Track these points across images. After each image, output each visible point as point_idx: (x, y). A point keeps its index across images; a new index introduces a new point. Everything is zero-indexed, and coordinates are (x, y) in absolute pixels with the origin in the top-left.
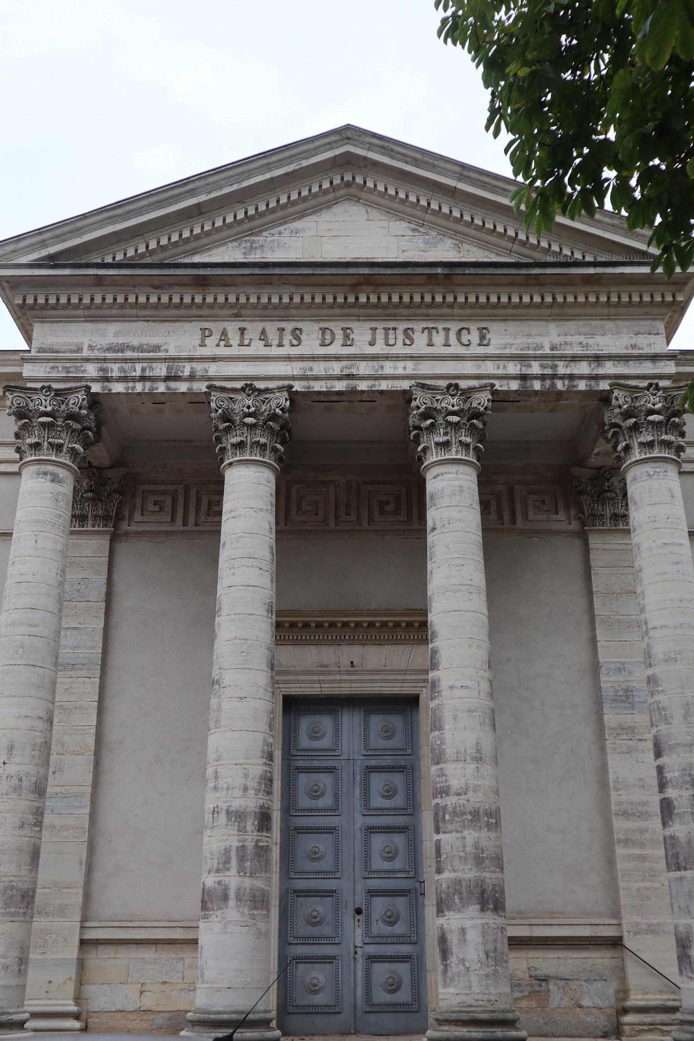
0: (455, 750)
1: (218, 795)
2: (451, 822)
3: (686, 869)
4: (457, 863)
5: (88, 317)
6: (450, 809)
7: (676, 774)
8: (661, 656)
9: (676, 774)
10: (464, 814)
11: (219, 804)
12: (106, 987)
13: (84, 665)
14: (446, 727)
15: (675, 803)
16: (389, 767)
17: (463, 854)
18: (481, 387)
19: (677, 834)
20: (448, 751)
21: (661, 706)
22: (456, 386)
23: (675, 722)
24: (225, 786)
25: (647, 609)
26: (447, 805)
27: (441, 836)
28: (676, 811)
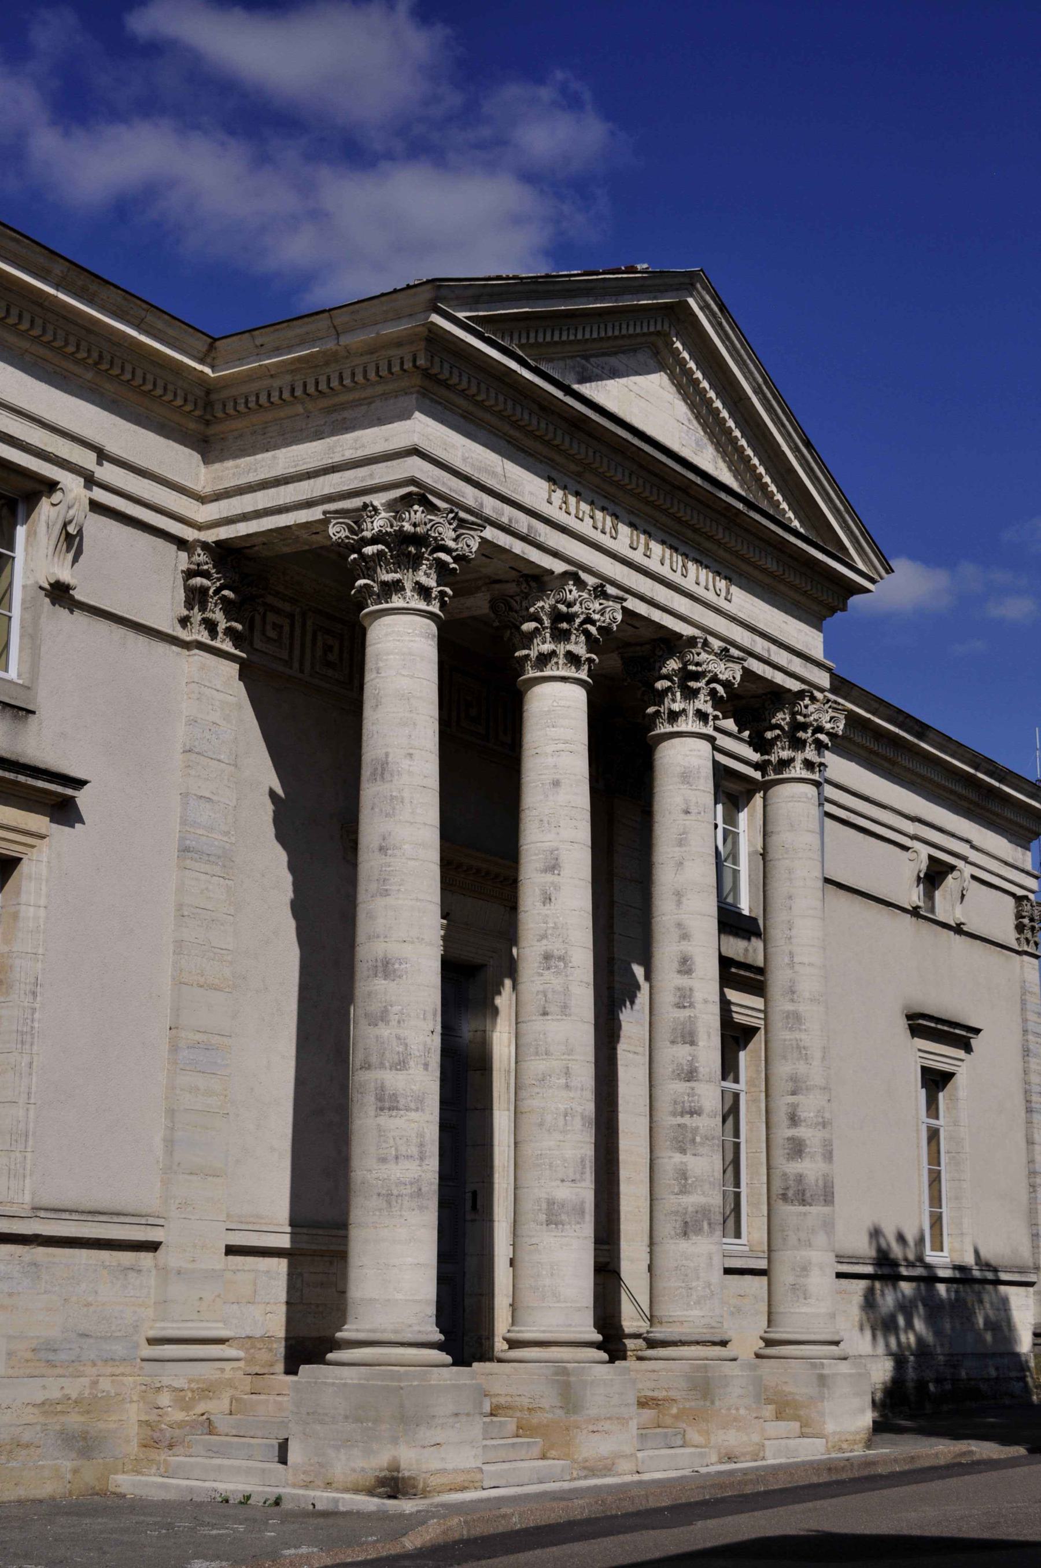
0: (708, 1070)
1: (572, 1095)
2: (702, 1144)
3: (811, 1205)
4: (707, 1187)
5: (510, 437)
6: (702, 1131)
7: (812, 1114)
8: (807, 995)
9: (812, 1114)
10: (713, 1138)
11: (574, 1106)
12: (235, 1306)
13: (219, 857)
14: (700, 1044)
15: (808, 1142)
16: (767, 1096)
17: (712, 1179)
18: (738, 658)
19: (806, 1172)
20: (701, 1069)
21: (802, 1044)
22: (728, 650)
23: (815, 1063)
24: (579, 1085)
25: (794, 940)
26: (697, 1128)
27: (688, 1158)
28: (807, 1150)
